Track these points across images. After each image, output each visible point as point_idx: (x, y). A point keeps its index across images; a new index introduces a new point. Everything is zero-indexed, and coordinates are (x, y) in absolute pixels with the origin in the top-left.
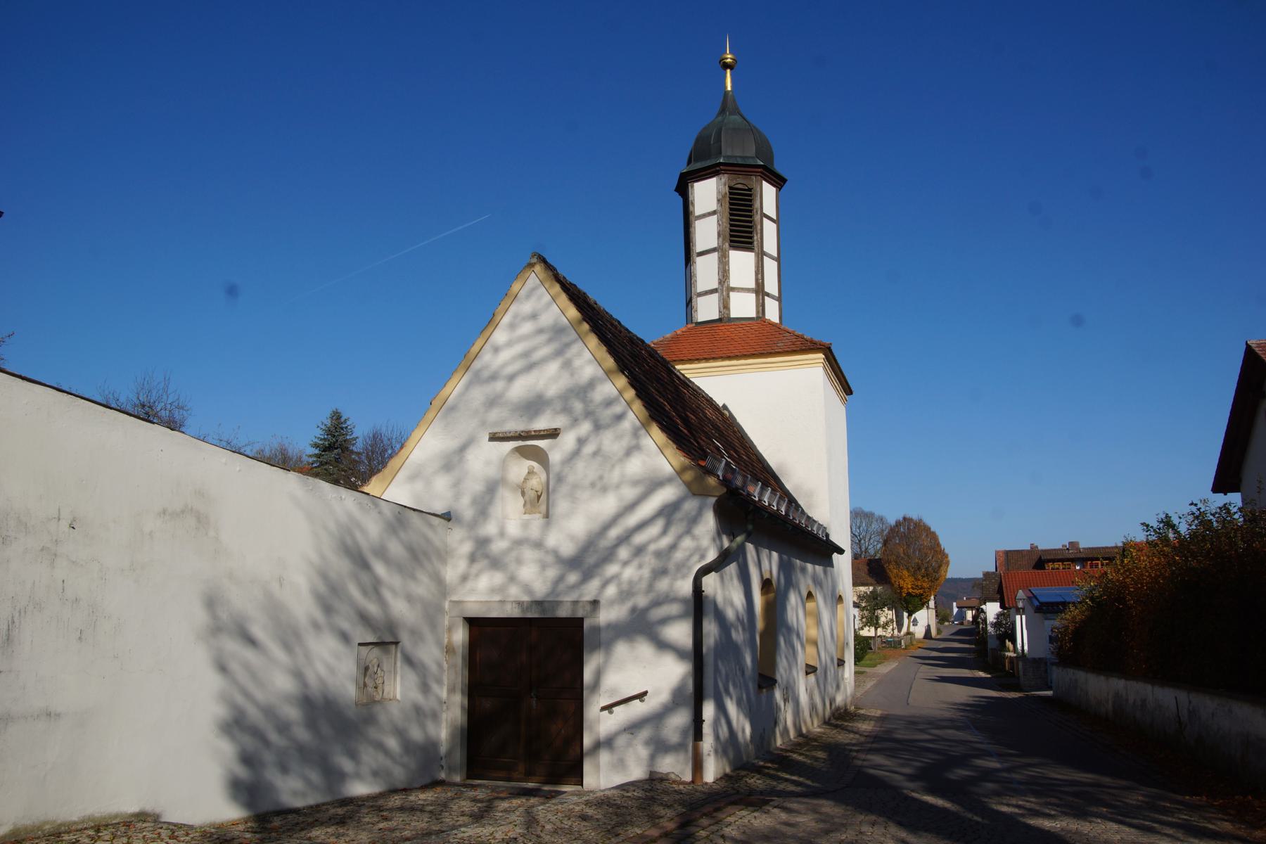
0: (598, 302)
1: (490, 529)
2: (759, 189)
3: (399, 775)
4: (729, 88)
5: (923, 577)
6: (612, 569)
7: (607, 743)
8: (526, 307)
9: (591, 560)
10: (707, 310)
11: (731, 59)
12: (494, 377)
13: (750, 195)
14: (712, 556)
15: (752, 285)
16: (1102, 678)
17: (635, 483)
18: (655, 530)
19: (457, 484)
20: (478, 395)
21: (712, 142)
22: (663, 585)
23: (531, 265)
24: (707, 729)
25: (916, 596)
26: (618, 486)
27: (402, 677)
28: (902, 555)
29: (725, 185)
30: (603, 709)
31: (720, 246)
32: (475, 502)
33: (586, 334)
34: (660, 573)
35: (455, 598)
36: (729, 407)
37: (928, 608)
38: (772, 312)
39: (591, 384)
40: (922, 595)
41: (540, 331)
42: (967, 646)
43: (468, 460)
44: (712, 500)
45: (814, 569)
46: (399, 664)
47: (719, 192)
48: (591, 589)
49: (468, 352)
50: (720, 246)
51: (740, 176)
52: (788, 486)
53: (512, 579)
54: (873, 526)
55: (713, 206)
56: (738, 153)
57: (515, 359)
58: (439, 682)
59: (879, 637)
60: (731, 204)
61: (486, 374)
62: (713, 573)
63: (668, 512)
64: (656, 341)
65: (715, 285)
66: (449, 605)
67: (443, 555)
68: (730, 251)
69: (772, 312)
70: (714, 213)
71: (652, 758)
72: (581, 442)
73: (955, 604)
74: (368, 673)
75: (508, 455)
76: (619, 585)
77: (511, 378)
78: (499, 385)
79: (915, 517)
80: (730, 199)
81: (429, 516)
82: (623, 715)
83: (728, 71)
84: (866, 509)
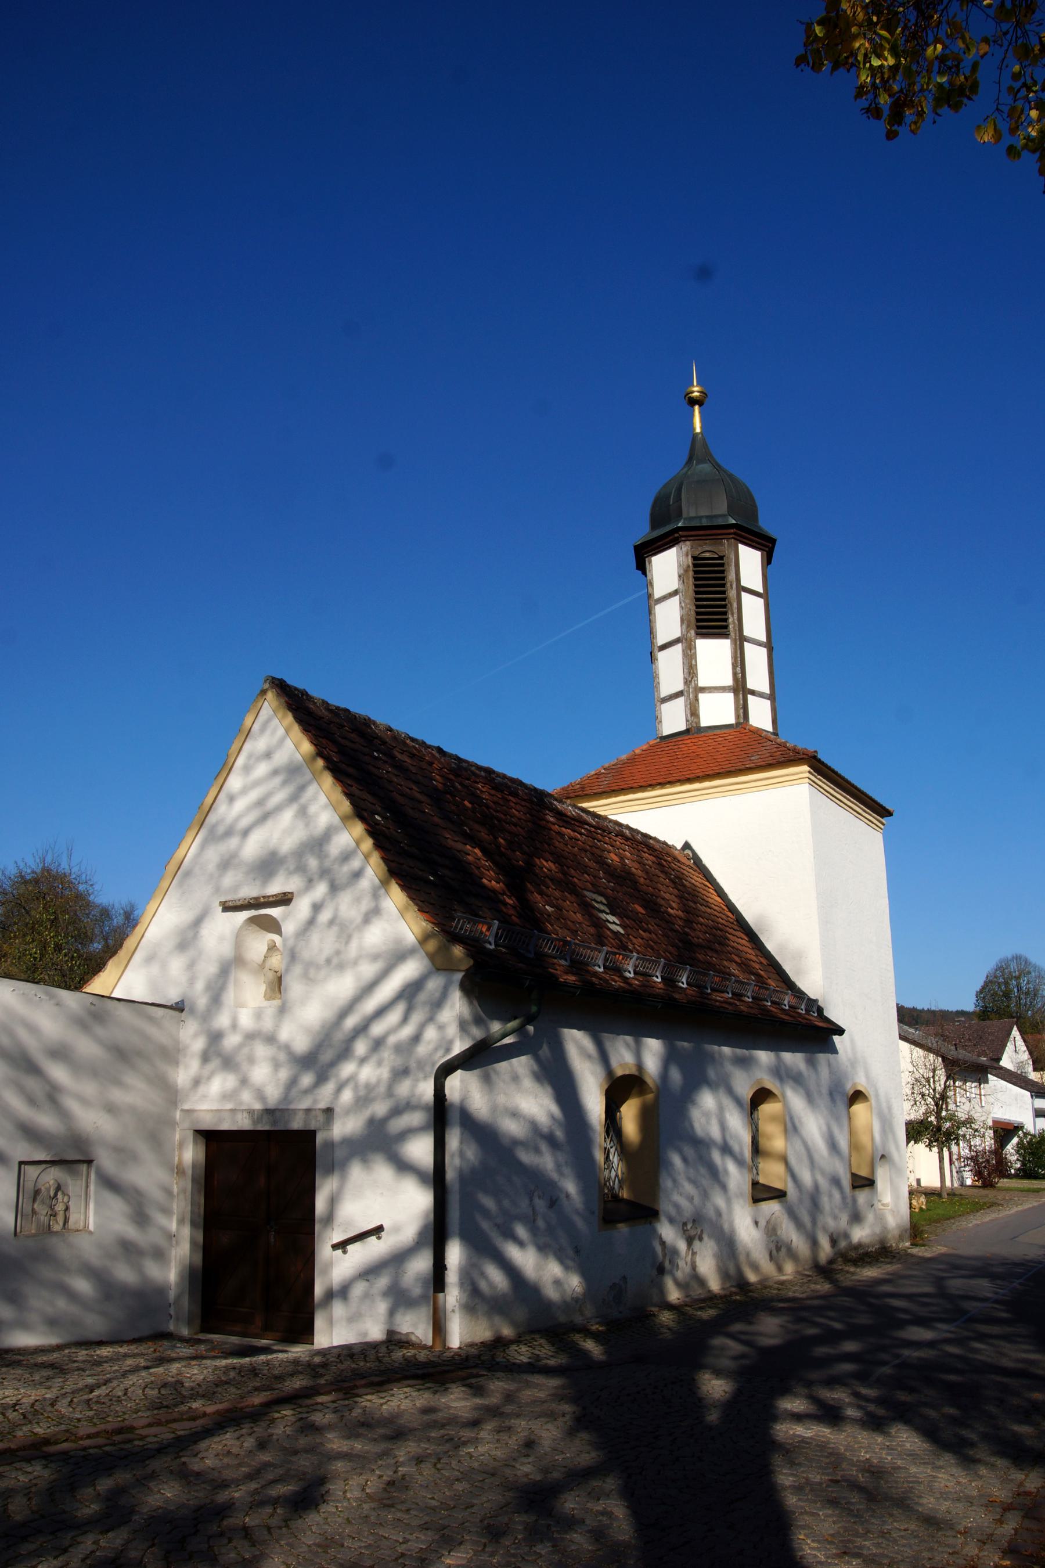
0: (393, 727)
1: (223, 1021)
2: (732, 556)
3: (95, 1324)
4: (698, 430)
6: (347, 1069)
7: (343, 1292)
8: (258, 744)
9: (327, 1056)
11: (698, 392)
12: (229, 833)
13: (722, 565)
14: (458, 1047)
15: (729, 682)
17: (375, 957)
18: (394, 1017)
19: (191, 966)
20: (213, 855)
21: (671, 503)
22: (404, 1089)
23: (263, 692)
24: (452, 1277)
26: (355, 963)
27: (97, 1203)
30: (335, 1247)
32: (208, 987)
33: (321, 772)
34: (401, 1073)
35: (186, 1107)
38: (761, 716)
39: (327, 836)
41: (275, 772)
43: (202, 937)
44: (459, 976)
45: (778, 1058)
46: (92, 1187)
47: (679, 566)
48: (325, 1095)
49: (202, 804)
51: (707, 542)
52: (770, 946)
53: (244, 1082)
55: (674, 584)
56: (704, 512)
57: (249, 809)
58: (166, 1211)
60: (696, 579)
61: (221, 829)
62: (459, 1071)
63: (410, 993)
64: (606, 765)
65: (680, 686)
66: (180, 1115)
67: (172, 1054)
69: (761, 716)
70: (675, 593)
71: (392, 1313)
72: (317, 908)
74: (39, 1199)
75: (241, 927)
76: (356, 1088)
77: (246, 833)
78: (234, 842)
80: (695, 572)
81: (144, 1005)
82: (360, 1255)
83: (697, 408)
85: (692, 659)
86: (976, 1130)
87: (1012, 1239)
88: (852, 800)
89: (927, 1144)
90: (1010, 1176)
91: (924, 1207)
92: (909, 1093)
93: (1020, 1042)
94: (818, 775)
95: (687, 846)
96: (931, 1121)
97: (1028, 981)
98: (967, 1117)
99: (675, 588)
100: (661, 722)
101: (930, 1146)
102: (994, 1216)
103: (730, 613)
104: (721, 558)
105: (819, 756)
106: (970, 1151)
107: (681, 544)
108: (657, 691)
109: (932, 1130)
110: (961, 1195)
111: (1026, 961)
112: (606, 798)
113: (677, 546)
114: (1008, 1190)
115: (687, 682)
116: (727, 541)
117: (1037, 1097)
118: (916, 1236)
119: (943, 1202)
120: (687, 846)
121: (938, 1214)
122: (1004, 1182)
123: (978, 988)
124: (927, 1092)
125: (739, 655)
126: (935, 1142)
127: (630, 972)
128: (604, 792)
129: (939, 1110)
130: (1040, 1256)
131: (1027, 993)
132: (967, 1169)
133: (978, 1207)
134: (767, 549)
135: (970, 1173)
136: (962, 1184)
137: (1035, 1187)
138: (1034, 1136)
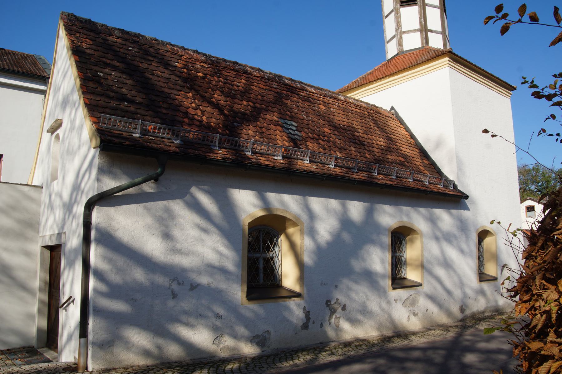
10: (391, 50)
15: (418, 26)
68: (401, 9)
88: (485, 79)
94: (457, 63)
95: (392, 108)
105: (454, 52)
112: (357, 90)
115: (396, 31)
120: (392, 108)
125: (422, 13)
127: (427, 182)
128: (355, 88)
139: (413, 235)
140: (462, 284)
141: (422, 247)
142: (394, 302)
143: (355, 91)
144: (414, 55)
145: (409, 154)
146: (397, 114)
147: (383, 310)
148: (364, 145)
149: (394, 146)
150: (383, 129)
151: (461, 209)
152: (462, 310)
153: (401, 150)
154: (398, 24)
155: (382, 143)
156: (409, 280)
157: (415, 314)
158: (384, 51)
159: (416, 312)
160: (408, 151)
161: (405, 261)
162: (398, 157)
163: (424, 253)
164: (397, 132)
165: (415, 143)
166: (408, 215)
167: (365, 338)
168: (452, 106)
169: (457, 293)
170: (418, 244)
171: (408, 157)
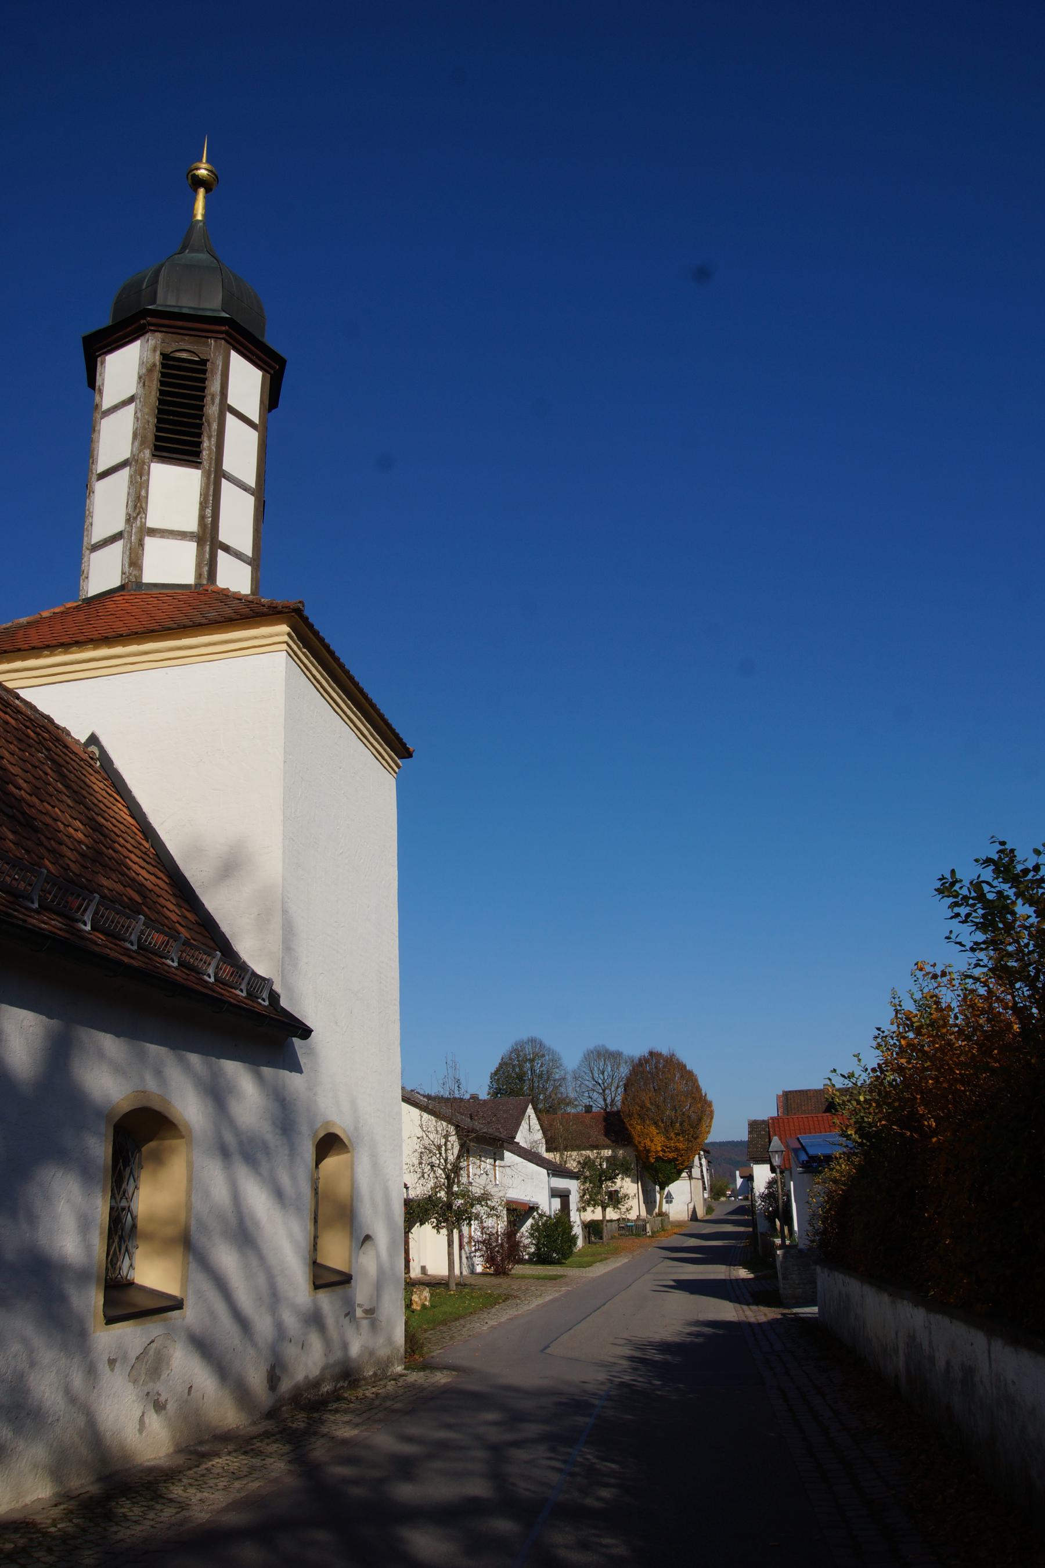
2: (220, 363)
5: (677, 1134)
15: (192, 525)
16: (886, 1298)
25: (670, 1161)
28: (649, 1105)
29: (155, 350)
31: (134, 456)
36: (101, 739)
37: (690, 1177)
40: (676, 1159)
42: (742, 1229)
47: (142, 364)
50: (134, 456)
51: (186, 338)
54: (622, 1069)
59: (608, 1221)
60: (162, 383)
65: (119, 525)
70: (131, 400)
73: (738, 1173)
79: (665, 1051)
80: (163, 375)
83: (201, 192)
84: (612, 1047)
85: (141, 488)
86: (493, 1208)
87: (542, 1351)
89: (434, 1224)
90: (521, 1261)
91: (427, 1303)
92: (416, 1162)
93: (534, 1121)
94: (305, 647)
96: (440, 1197)
97: (542, 1064)
98: (482, 1192)
99: (132, 394)
100: (87, 578)
101: (438, 1228)
102: (513, 1312)
103: (205, 434)
104: (204, 362)
106: (482, 1233)
107: (147, 336)
108: (87, 536)
109: (441, 1208)
110: (471, 1285)
111: (541, 1044)
113: (142, 338)
114: (522, 1278)
115: (129, 520)
116: (215, 341)
117: (554, 1175)
118: (413, 1351)
119: (450, 1295)
121: (445, 1313)
122: (518, 1269)
123: (493, 1069)
124: (438, 1162)
125: (211, 493)
126: (444, 1222)
129: (449, 1187)
130: (602, 1383)
131: (540, 1076)
132: (478, 1254)
133: (492, 1301)
134: (272, 372)
135: (481, 1259)
136: (472, 1272)
137: (551, 1273)
138: (549, 1217)
139: (163, 1139)
140: (274, 1298)
141: (190, 1180)
142: (107, 1368)
143: (88, 650)
144: (176, 602)
145: (148, 884)
146: (105, 758)
147: (72, 1399)
148: (36, 830)
149: (111, 851)
150: (80, 795)
151: (284, 1069)
152: (273, 1379)
153: (129, 869)
154: (138, 503)
155: (80, 835)
156: (143, 1289)
157: (159, 1407)
158: (76, 572)
159: (162, 1399)
160: (143, 873)
161: (134, 1226)
162: (125, 886)
163: (193, 1199)
164: (112, 814)
165: (157, 854)
166: (159, 1073)
167: (16, 1516)
168: (285, 762)
169: (263, 1325)
170: (176, 1169)
171: (148, 892)
